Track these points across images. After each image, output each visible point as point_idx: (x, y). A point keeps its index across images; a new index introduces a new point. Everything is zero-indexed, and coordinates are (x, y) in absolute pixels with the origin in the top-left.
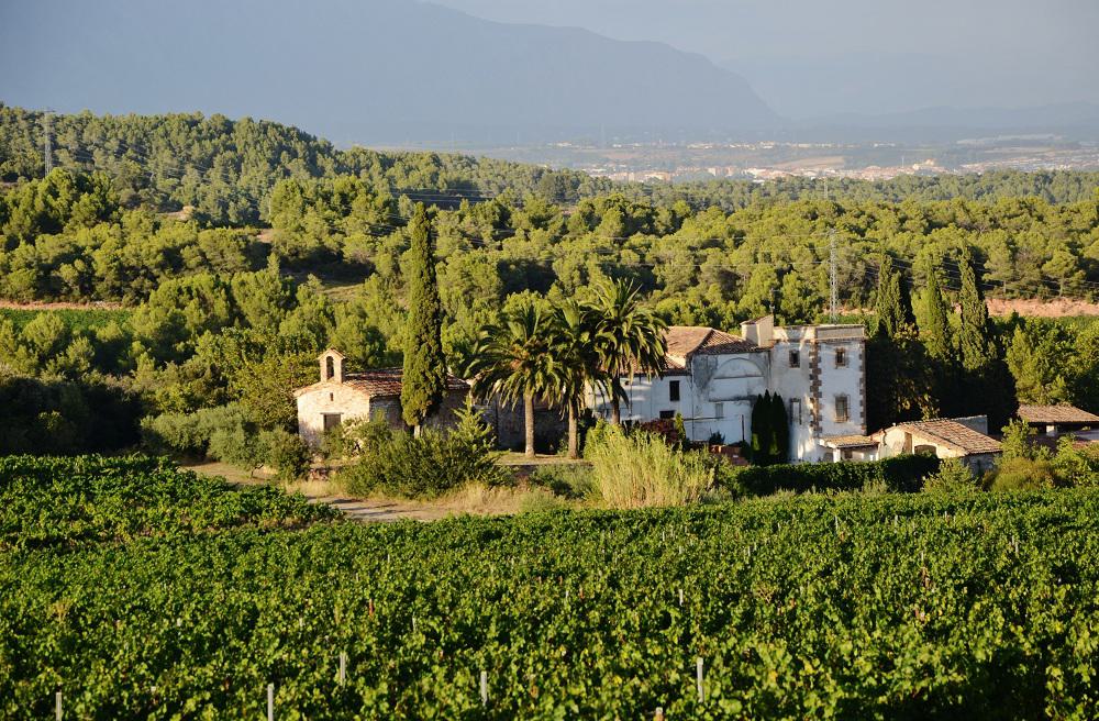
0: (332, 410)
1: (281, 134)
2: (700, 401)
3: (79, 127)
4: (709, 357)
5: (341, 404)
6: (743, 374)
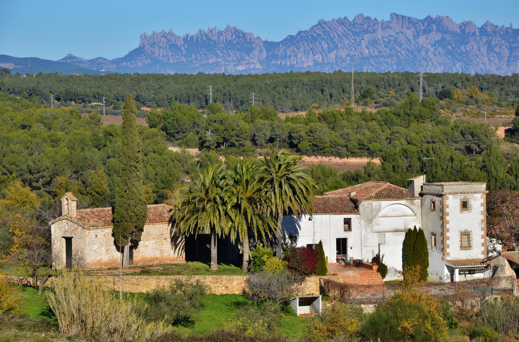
2: (366, 231)
4: (374, 202)
6: (401, 214)
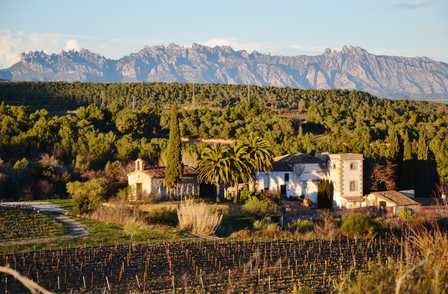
0: (139, 182)
1: (363, 94)
3: (307, 93)
5: (142, 180)
